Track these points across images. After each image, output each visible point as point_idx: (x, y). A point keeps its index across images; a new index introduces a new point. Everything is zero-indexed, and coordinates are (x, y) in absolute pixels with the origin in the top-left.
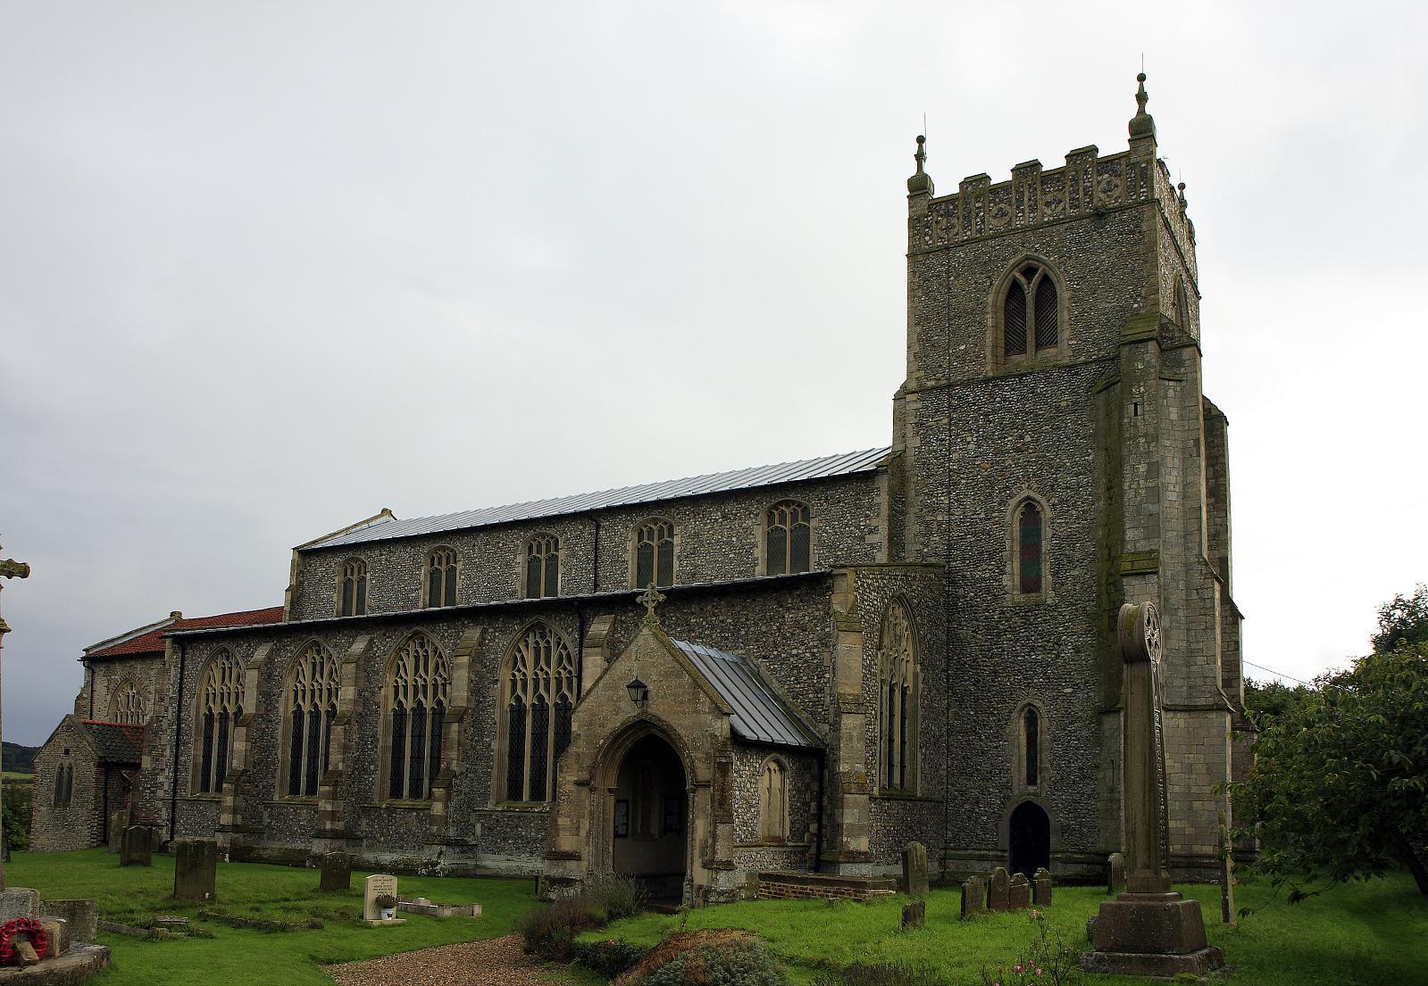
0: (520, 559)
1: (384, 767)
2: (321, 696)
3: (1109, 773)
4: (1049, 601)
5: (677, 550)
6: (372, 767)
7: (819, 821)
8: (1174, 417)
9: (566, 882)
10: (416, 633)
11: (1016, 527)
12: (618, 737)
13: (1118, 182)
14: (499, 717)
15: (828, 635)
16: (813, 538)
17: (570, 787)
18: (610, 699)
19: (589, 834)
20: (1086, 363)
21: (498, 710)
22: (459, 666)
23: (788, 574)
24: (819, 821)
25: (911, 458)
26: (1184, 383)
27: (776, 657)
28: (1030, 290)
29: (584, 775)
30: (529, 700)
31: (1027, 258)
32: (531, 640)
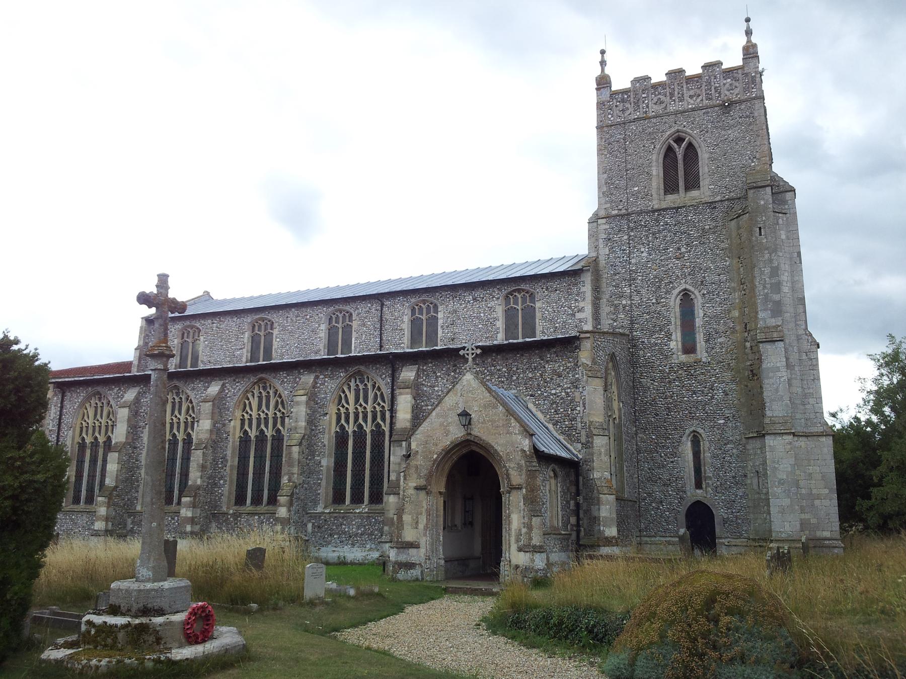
0: (246, 335)
1: (231, 481)
2: (87, 431)
3: (755, 481)
4: (704, 360)
5: (440, 322)
6: (222, 482)
7: (578, 516)
8: (783, 237)
9: (410, 566)
10: (261, 379)
11: (678, 309)
12: (448, 452)
13: (737, 85)
14: (327, 439)
15: (578, 380)
16: (538, 315)
17: (411, 491)
18: (441, 424)
19: (426, 528)
20: (721, 201)
21: (326, 436)
22: (298, 403)
23: (520, 340)
24: (578, 516)
25: (602, 262)
26: (788, 215)
27: (539, 395)
28: (680, 152)
29: (422, 482)
30: (350, 428)
31: (678, 131)
32: (352, 384)
